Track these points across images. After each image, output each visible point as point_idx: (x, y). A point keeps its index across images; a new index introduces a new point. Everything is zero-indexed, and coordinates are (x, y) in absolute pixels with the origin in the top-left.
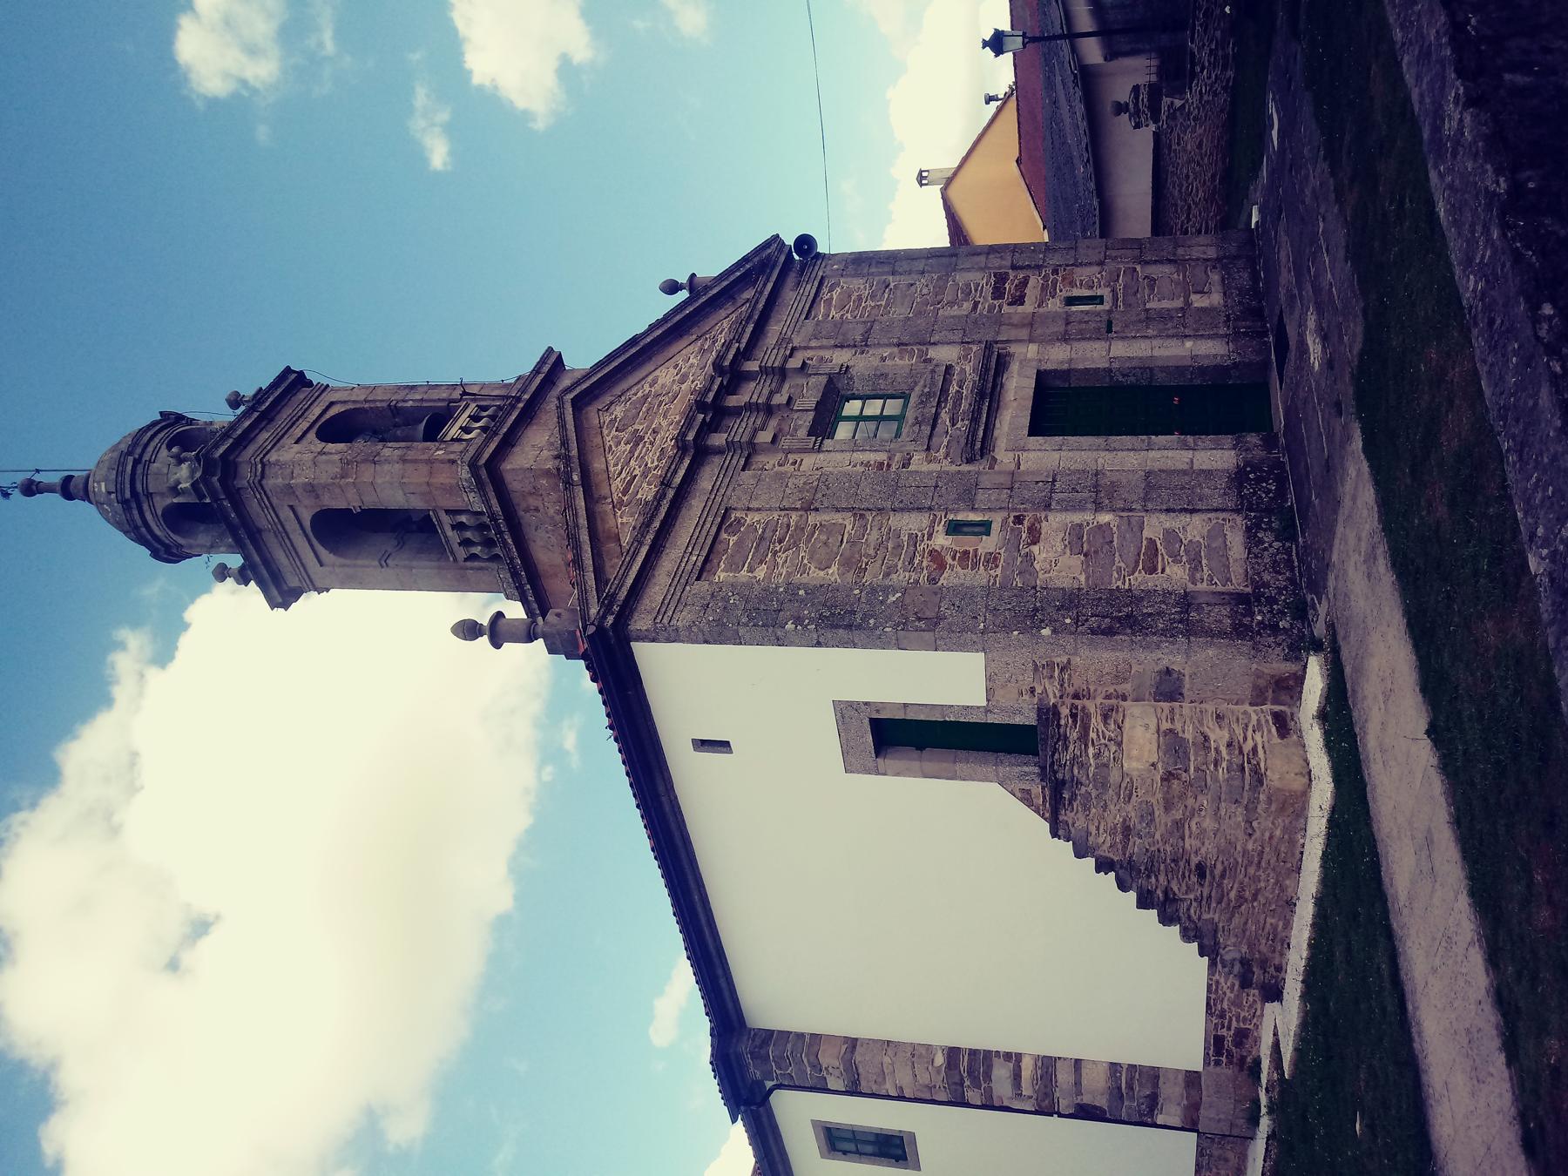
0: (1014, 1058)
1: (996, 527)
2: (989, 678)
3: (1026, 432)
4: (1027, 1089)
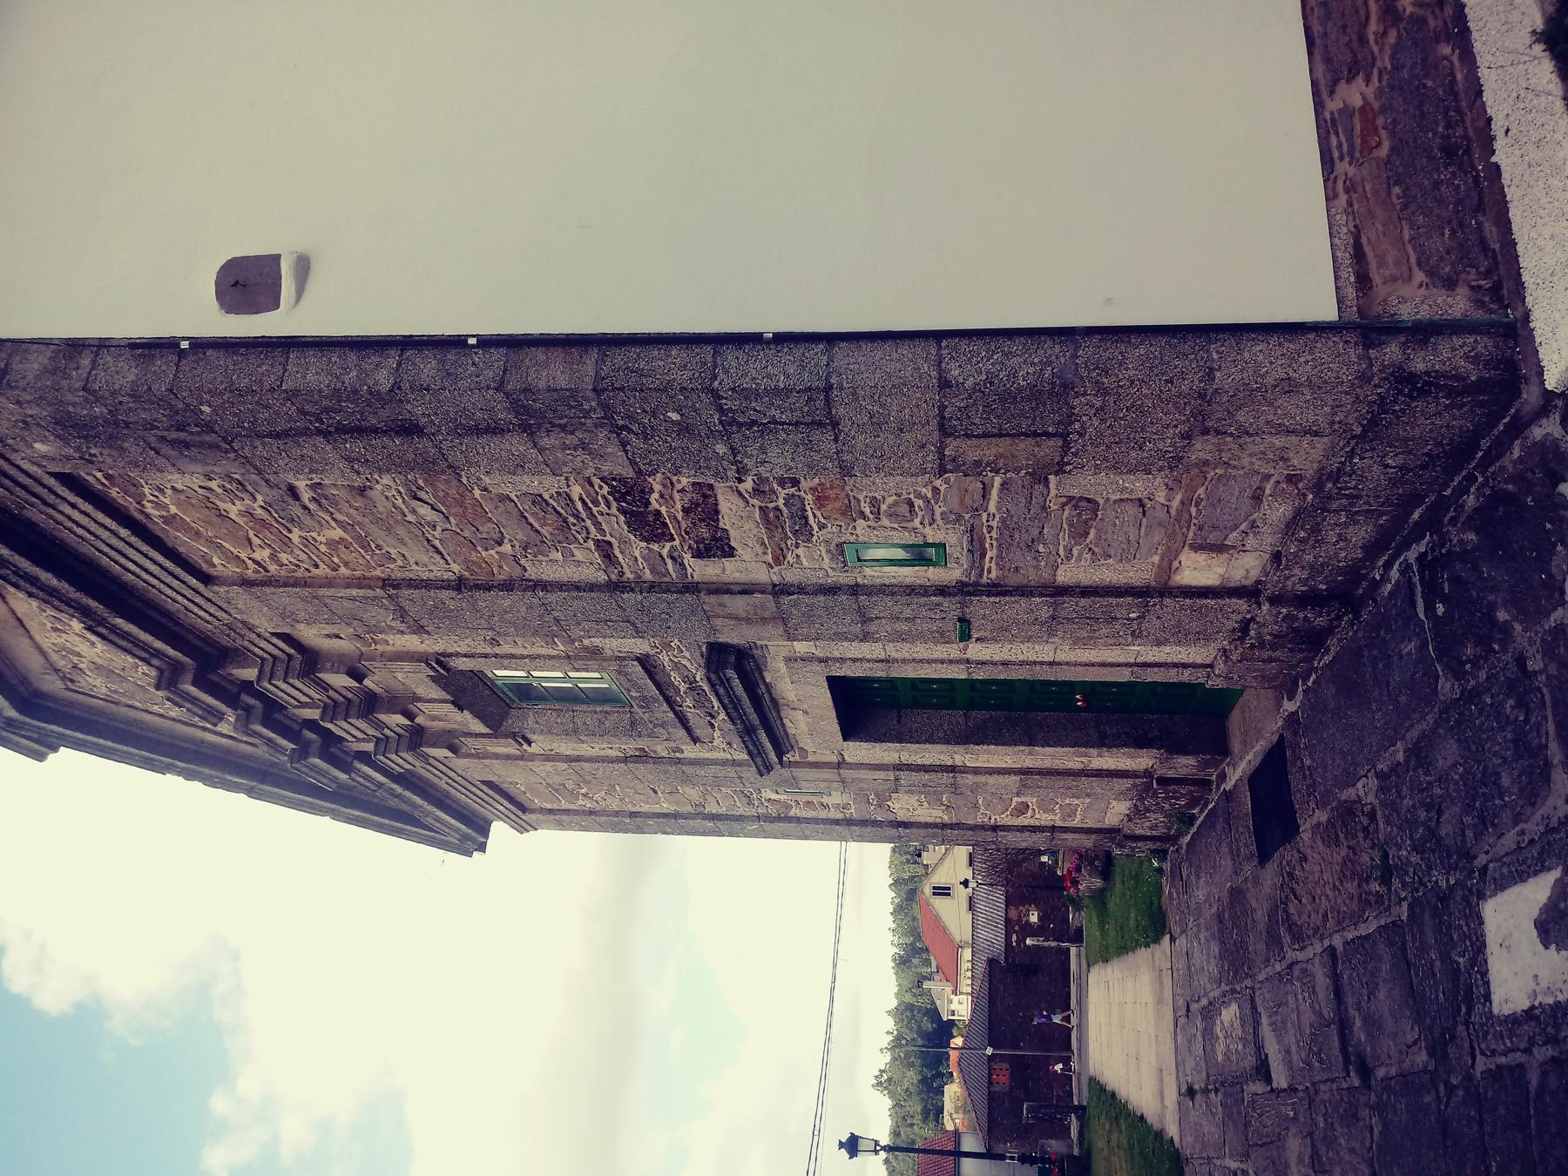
3: (840, 738)
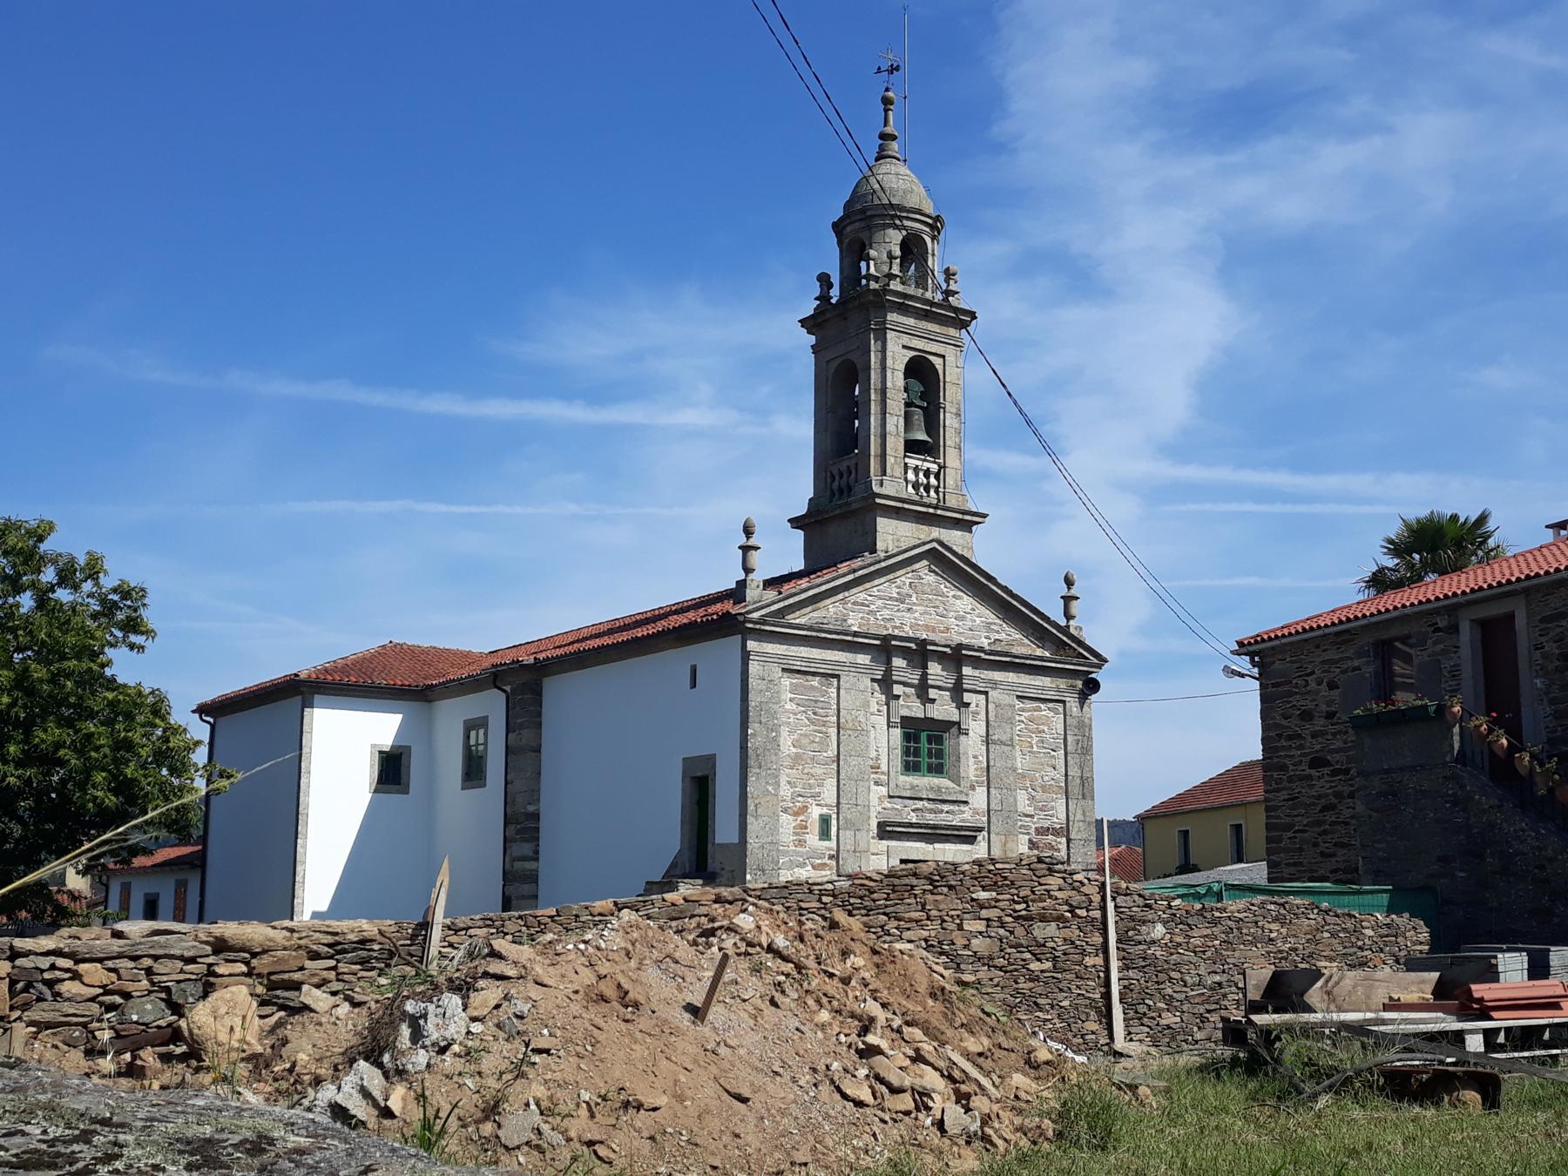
0: (535, 857)
1: (826, 843)
4: (518, 865)
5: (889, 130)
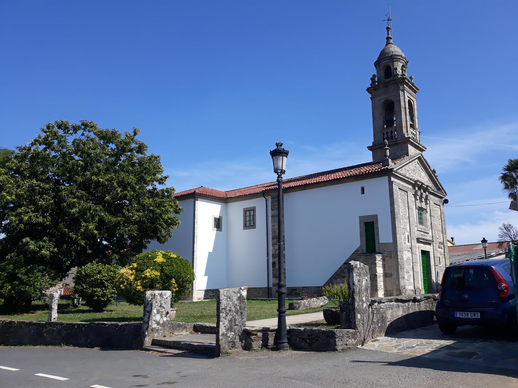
2: (386, 243)
5: (390, 36)
